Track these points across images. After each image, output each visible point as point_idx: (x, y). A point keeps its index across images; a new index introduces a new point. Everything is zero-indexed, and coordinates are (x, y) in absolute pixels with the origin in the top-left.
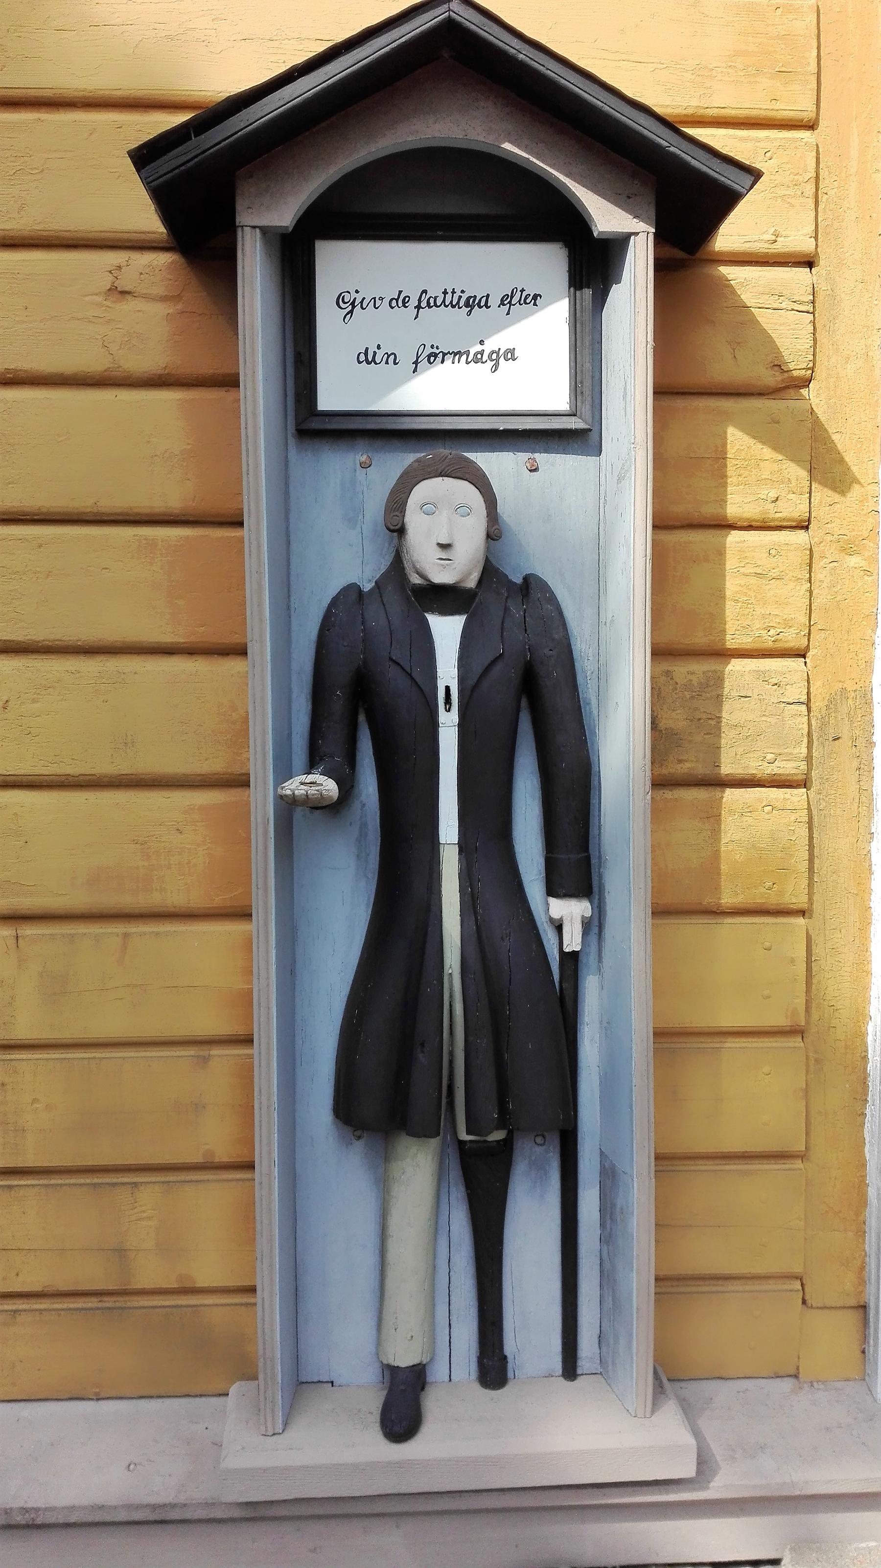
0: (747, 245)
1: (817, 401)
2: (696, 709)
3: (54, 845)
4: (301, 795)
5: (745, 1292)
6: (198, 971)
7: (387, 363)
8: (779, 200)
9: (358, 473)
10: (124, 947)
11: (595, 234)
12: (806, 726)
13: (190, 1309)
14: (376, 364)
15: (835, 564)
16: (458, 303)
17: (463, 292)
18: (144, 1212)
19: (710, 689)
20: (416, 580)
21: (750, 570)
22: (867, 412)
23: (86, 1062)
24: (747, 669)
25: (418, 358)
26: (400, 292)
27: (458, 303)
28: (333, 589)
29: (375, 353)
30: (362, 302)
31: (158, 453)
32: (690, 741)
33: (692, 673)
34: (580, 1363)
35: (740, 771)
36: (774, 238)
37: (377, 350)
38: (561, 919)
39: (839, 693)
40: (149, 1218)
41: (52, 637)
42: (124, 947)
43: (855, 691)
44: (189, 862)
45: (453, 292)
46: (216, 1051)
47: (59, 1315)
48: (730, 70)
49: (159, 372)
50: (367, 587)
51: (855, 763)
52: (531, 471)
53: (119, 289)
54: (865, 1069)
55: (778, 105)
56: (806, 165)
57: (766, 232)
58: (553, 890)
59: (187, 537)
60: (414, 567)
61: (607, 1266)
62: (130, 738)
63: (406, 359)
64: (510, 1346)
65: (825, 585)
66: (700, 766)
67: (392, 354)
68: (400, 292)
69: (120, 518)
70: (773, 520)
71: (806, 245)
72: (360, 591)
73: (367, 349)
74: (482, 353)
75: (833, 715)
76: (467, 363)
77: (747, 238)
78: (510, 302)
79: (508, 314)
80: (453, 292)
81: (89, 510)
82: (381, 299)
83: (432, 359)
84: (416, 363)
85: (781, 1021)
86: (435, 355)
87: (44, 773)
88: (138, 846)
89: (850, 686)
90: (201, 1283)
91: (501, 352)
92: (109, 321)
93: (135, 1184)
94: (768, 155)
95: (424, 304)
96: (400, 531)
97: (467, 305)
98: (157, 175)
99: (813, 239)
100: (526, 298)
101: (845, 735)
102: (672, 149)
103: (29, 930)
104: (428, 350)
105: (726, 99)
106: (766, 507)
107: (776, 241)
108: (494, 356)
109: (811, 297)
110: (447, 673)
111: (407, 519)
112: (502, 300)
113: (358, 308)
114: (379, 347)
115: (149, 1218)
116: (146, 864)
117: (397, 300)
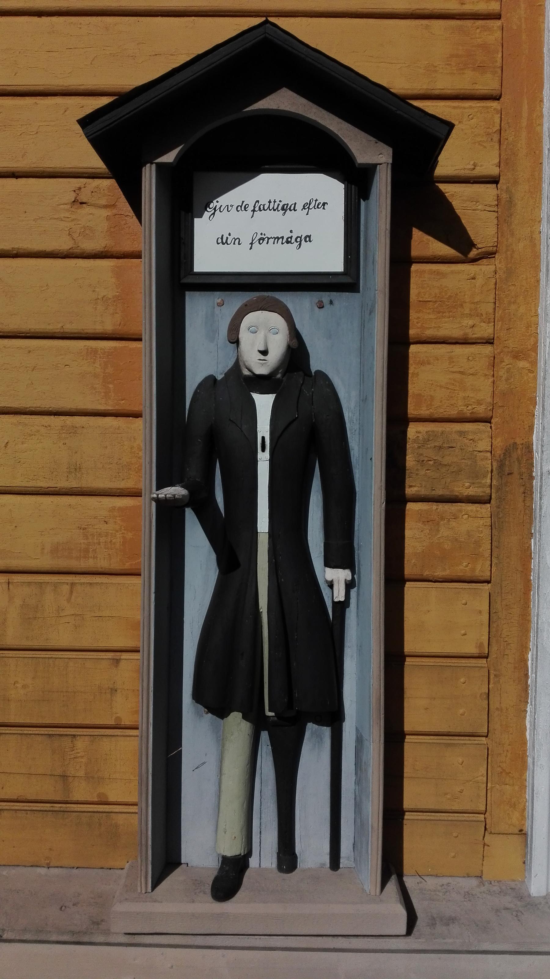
0: (457, 172)
1: (500, 266)
2: (422, 455)
4: (163, 497)
5: (448, 821)
7: (234, 244)
8: (477, 144)
9: (215, 310)
10: (71, 592)
11: (357, 165)
12: (490, 466)
13: (105, 814)
14: (228, 244)
15: (510, 366)
16: (277, 208)
17: (280, 201)
18: (79, 753)
19: (430, 442)
20: (246, 372)
21: (455, 369)
22: (531, 272)
23: (47, 660)
24: (454, 430)
25: (253, 241)
26: (243, 202)
27: (277, 208)
28: (199, 378)
29: (227, 238)
30: (220, 208)
31: (99, 297)
32: (417, 474)
33: (419, 432)
34: (342, 861)
35: (448, 493)
36: (473, 167)
37: (228, 237)
38: (332, 581)
39: (512, 446)
40: (82, 757)
41: (35, 405)
42: (71, 592)
43: (522, 444)
44: (111, 541)
45: (275, 202)
46: (125, 656)
47: (27, 814)
48: (447, 66)
49: (102, 250)
50: (219, 377)
51: (522, 489)
52: (319, 308)
53: (79, 201)
54: (527, 682)
55: (477, 87)
56: (494, 123)
57: (469, 164)
58: (328, 563)
59: (115, 348)
60: (245, 365)
61: (358, 798)
62: (78, 466)
63: (246, 241)
65: (503, 378)
66: (423, 490)
67: (238, 238)
68: (243, 202)
69: (76, 335)
70: (472, 339)
71: (494, 171)
72: (215, 380)
73: (223, 235)
74: (291, 237)
75: (508, 459)
76: (282, 243)
77: (457, 168)
78: (308, 208)
79: (307, 214)
80: (275, 202)
81: (58, 331)
82: (232, 206)
83: (261, 241)
84: (252, 244)
85: (472, 650)
86: (263, 239)
87: (27, 486)
88: (81, 531)
89: (519, 441)
90: (112, 799)
91: (303, 237)
92: (73, 220)
93: (74, 736)
94: (470, 117)
95: (257, 209)
96: (236, 342)
97: (283, 209)
98: (93, 132)
99: (498, 168)
100: (318, 205)
101: (515, 470)
102: (398, 112)
104: (259, 236)
105: (444, 83)
106: (466, 331)
107: (474, 169)
108: (299, 240)
109: (496, 202)
110: (264, 428)
111: (240, 336)
112: (304, 206)
113: (218, 212)
114: (230, 234)
115: (82, 757)
116: (86, 541)
117: (241, 207)
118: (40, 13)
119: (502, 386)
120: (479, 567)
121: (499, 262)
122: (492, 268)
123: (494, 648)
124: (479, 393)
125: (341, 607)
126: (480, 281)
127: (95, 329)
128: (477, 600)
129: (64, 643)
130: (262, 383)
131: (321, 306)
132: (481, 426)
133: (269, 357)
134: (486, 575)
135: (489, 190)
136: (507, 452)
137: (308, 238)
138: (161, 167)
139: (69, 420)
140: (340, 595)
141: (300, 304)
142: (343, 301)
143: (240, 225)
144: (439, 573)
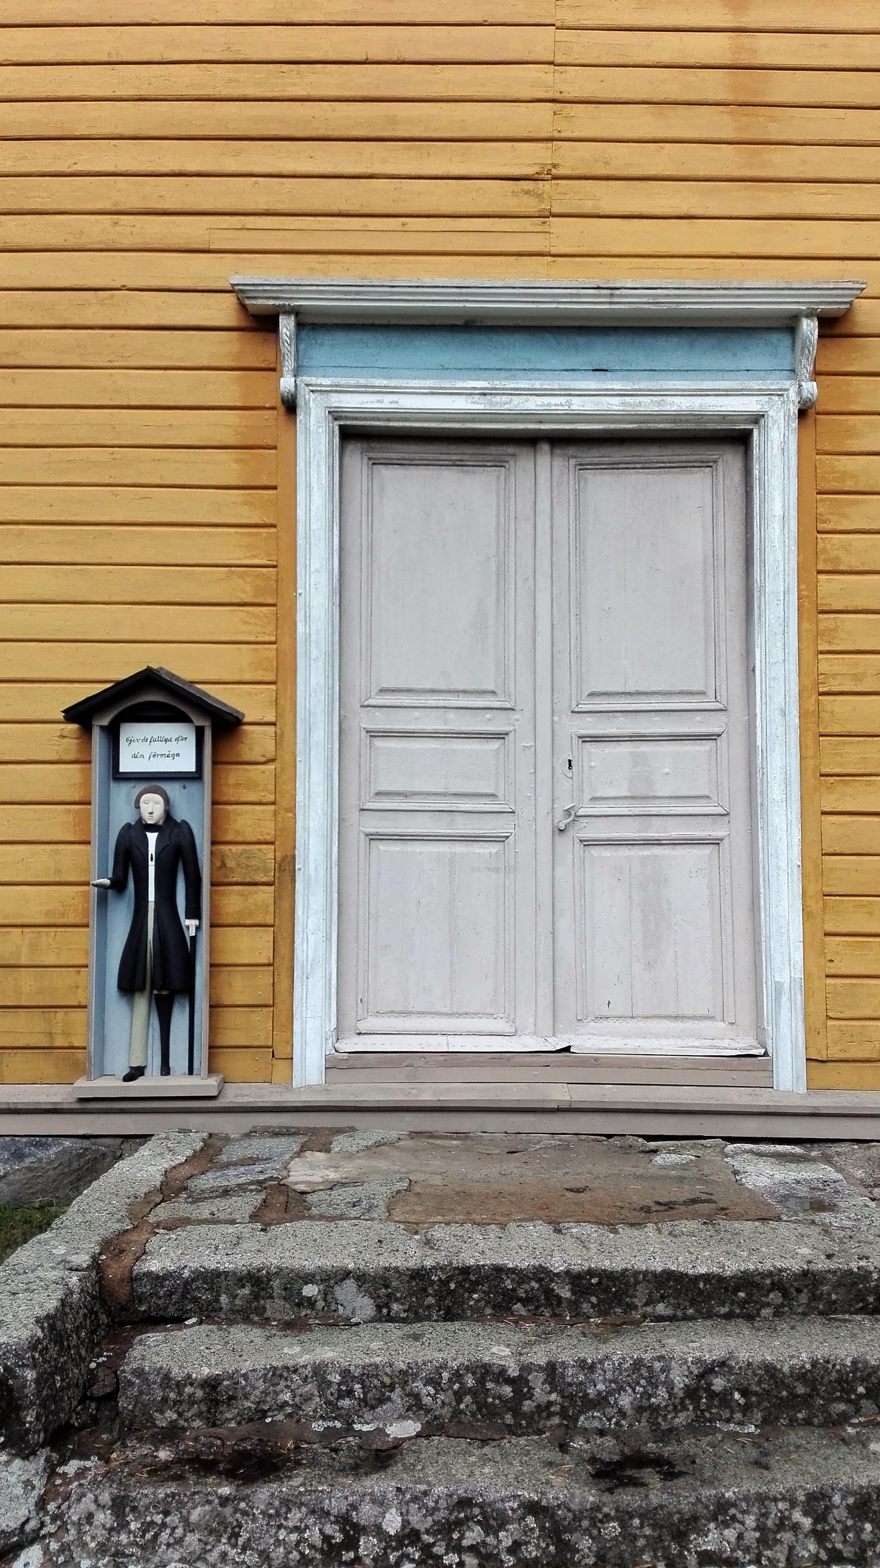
3: (36, 904)
6: (78, 945)
28: (122, 825)
50: (133, 823)
64: (171, 1064)
71: (273, 719)
101: (287, 868)
103: (26, 930)
118: (42, 641)
119: (280, 826)
120: (268, 918)
121: (277, 764)
122: (273, 767)
123: (277, 960)
124: (268, 830)
125: (194, 939)
126: (267, 773)
127: (9, 1103)
128: (267, 936)
129: (51, 963)
130: (152, 828)
131: (184, 788)
132: (270, 846)
133: (154, 815)
134: (271, 922)
135: (272, 728)
136: (283, 859)
137: (178, 755)
138: (102, 728)
139: (55, 847)
140: (192, 933)
141: (173, 789)
142: (193, 787)
143: (145, 749)
144: (248, 922)
